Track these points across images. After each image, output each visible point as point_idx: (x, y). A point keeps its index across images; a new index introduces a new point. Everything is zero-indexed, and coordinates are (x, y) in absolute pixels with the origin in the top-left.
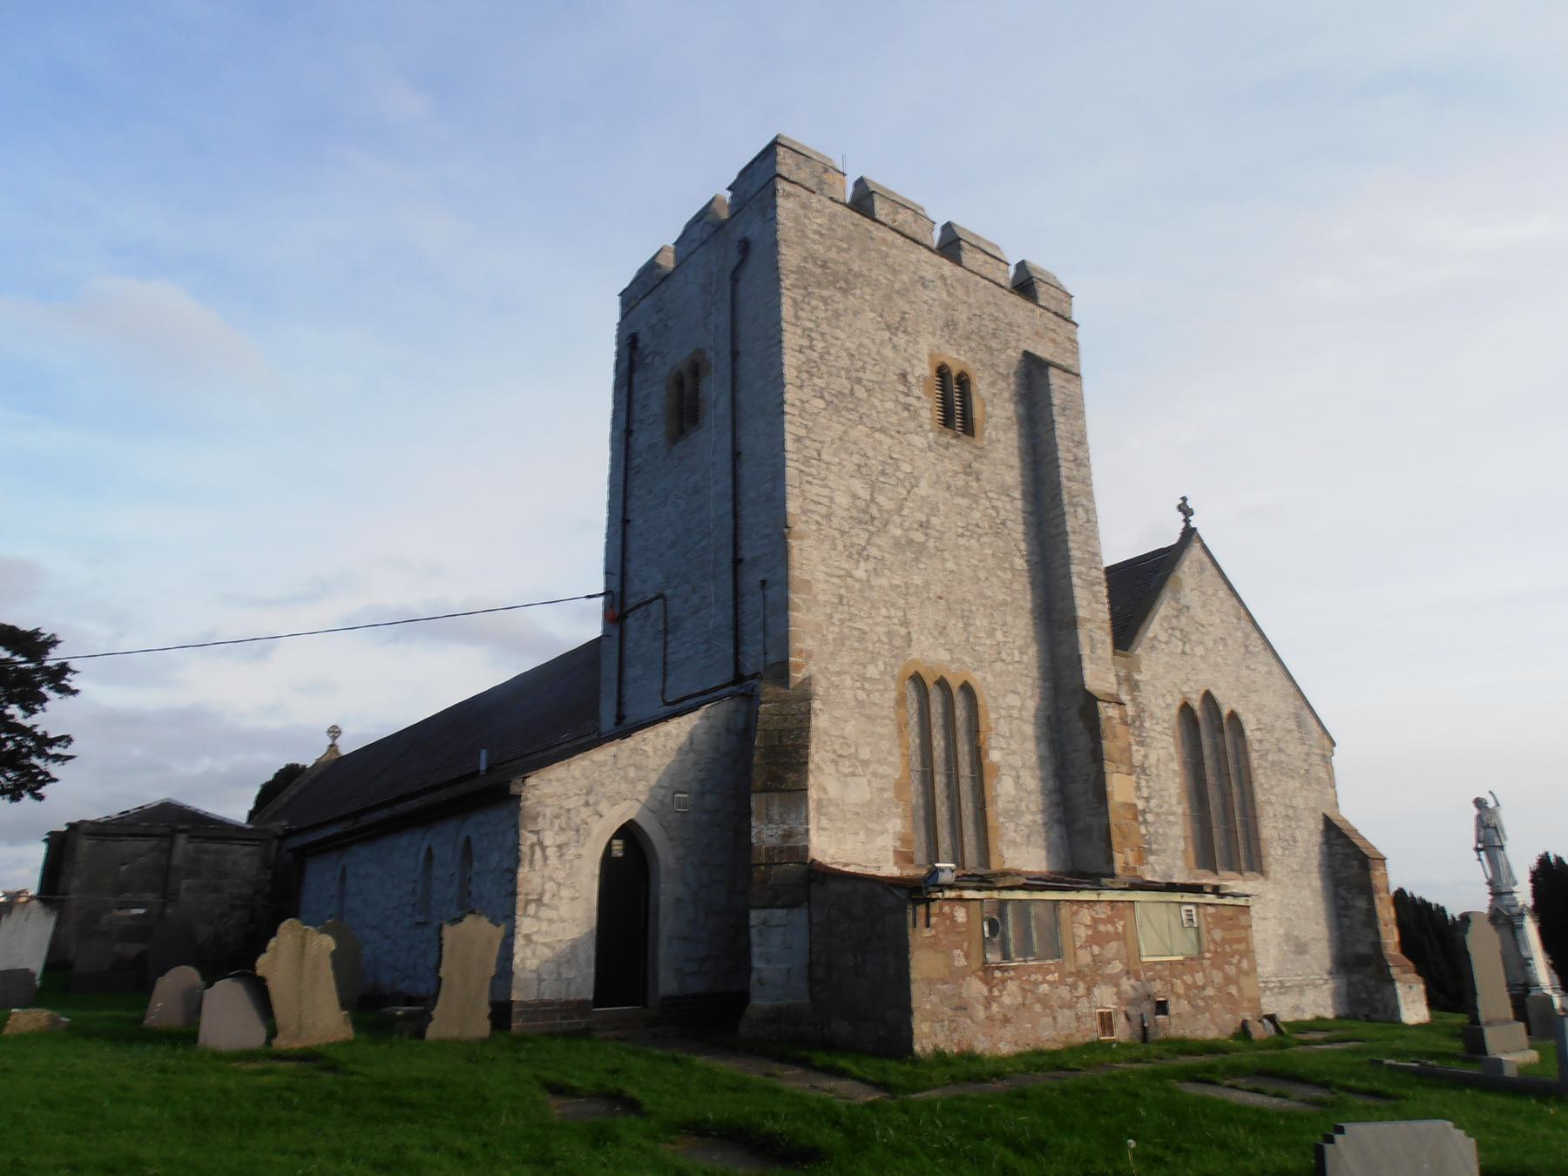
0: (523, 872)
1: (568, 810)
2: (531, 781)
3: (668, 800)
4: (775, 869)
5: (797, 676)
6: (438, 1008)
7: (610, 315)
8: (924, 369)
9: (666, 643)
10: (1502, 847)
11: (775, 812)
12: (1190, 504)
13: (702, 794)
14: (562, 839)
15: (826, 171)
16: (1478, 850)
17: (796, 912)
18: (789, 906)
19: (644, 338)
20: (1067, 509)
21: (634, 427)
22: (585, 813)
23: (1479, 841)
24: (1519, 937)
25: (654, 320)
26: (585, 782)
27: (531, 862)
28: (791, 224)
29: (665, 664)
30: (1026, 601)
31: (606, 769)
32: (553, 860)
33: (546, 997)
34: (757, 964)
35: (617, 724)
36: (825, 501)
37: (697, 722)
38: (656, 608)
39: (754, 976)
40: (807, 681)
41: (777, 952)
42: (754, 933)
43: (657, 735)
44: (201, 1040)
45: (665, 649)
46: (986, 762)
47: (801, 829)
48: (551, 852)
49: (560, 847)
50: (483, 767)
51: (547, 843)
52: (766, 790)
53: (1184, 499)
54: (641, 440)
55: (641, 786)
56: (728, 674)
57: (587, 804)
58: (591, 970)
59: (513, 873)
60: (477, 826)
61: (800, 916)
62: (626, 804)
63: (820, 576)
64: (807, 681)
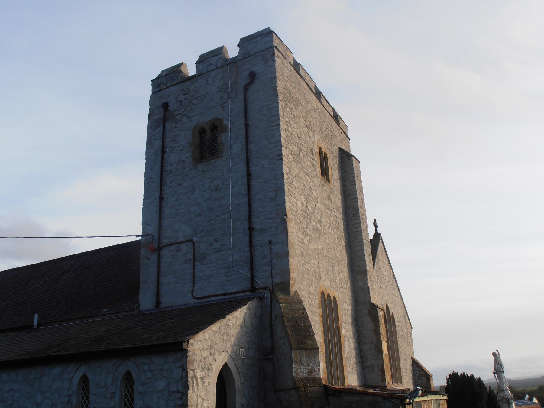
0: (190, 393)
2: (191, 341)
3: (238, 352)
4: (309, 389)
5: (293, 290)
8: (316, 150)
9: (194, 266)
10: (503, 372)
12: (377, 223)
14: (203, 374)
16: (494, 373)
19: (173, 105)
22: (211, 358)
23: (495, 369)
25: (182, 98)
26: (210, 342)
27: (193, 387)
28: (280, 71)
29: (194, 277)
30: (345, 260)
31: (217, 335)
35: (157, 307)
36: (295, 205)
40: (296, 292)
46: (341, 335)
47: (316, 368)
48: (199, 380)
49: (202, 379)
51: (198, 376)
53: (375, 220)
54: (172, 157)
55: (229, 345)
56: (246, 285)
59: (184, 394)
60: (144, 369)
62: (224, 354)
63: (296, 241)
64: (296, 292)
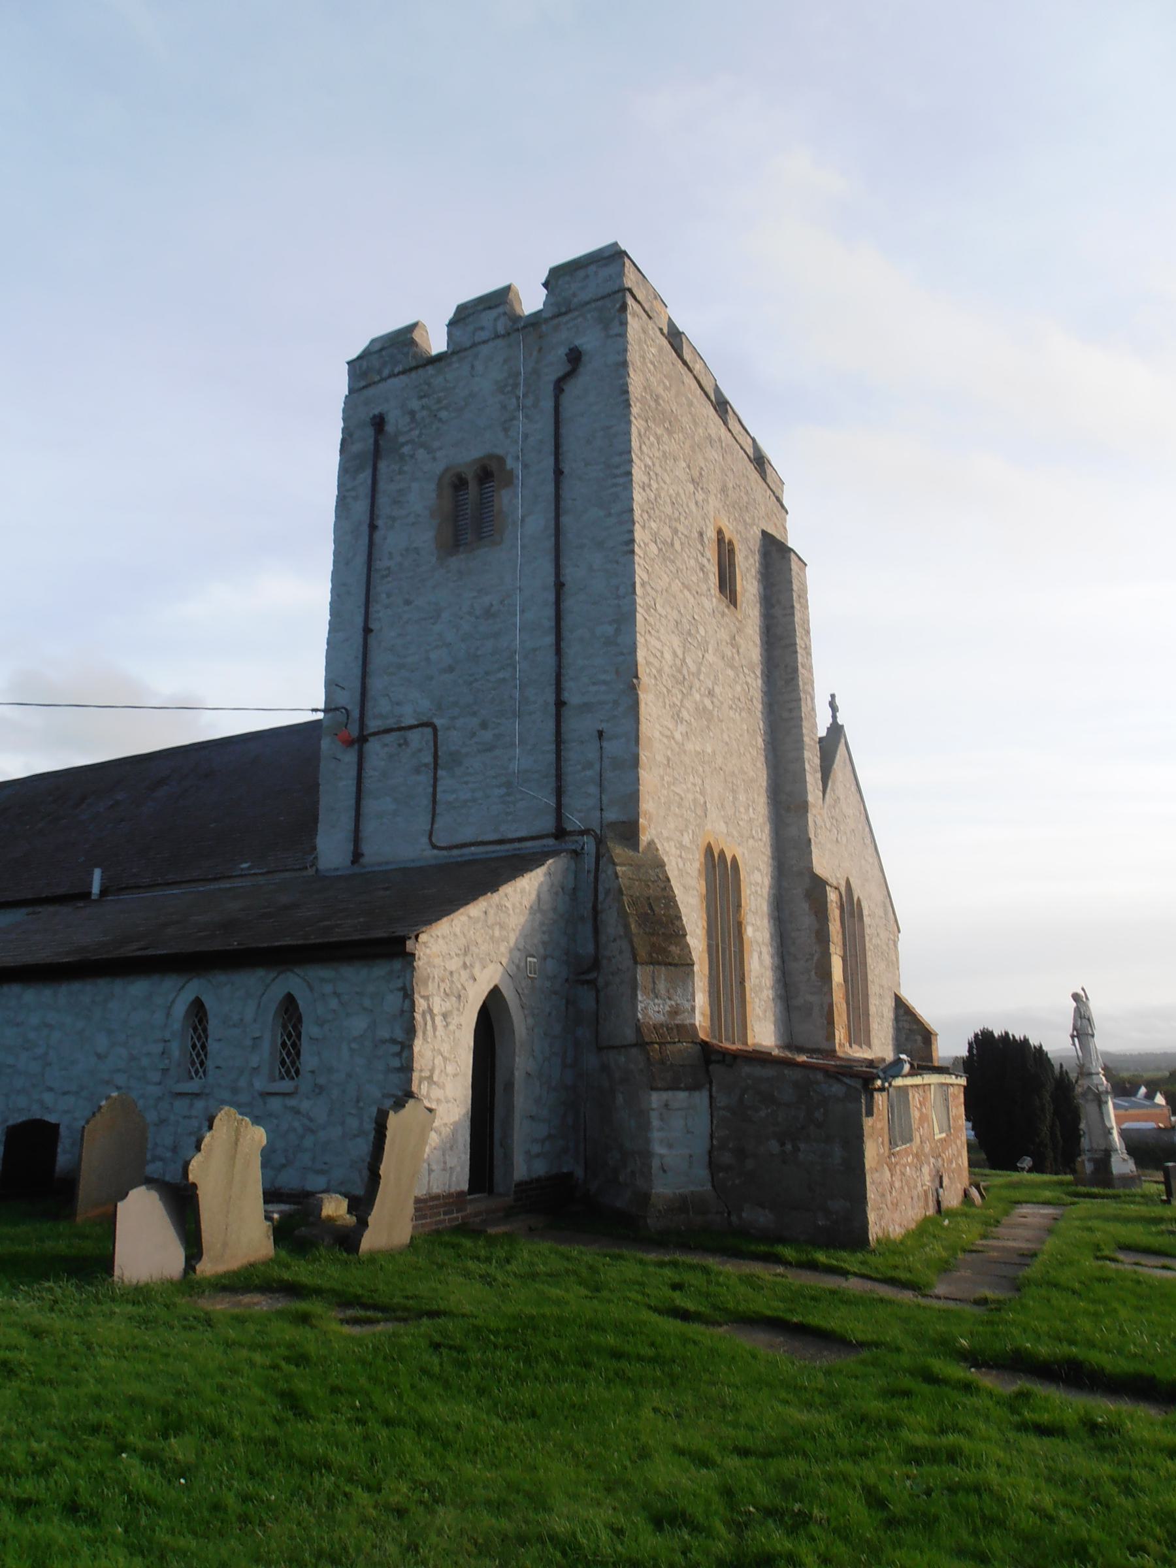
0: (418, 1045)
1: (451, 973)
2: (423, 938)
3: (523, 964)
5: (644, 838)
6: (374, 1213)
7: (340, 385)
9: (435, 780)
10: (1093, 1036)
11: (662, 987)
12: (838, 701)
13: (545, 958)
14: (447, 1006)
15: (656, 298)
17: (697, 1094)
18: (690, 1088)
20: (802, 695)
21: (380, 523)
22: (464, 974)
24: (1104, 1111)
27: (424, 1033)
29: (434, 802)
32: (440, 1031)
33: (436, 1190)
34: (659, 1149)
35: (353, 862)
37: (542, 879)
38: (416, 738)
39: (656, 1163)
40: (651, 843)
41: (675, 1141)
42: (654, 1116)
43: (515, 891)
44: (117, 1272)
45: (435, 786)
47: (687, 1006)
48: (438, 1019)
50: (96, 889)
51: (435, 1011)
52: (653, 963)
53: (833, 696)
54: (392, 541)
56: (547, 823)
57: (465, 966)
58: (466, 1157)
59: (405, 1046)
61: (701, 1099)
64: (651, 843)
